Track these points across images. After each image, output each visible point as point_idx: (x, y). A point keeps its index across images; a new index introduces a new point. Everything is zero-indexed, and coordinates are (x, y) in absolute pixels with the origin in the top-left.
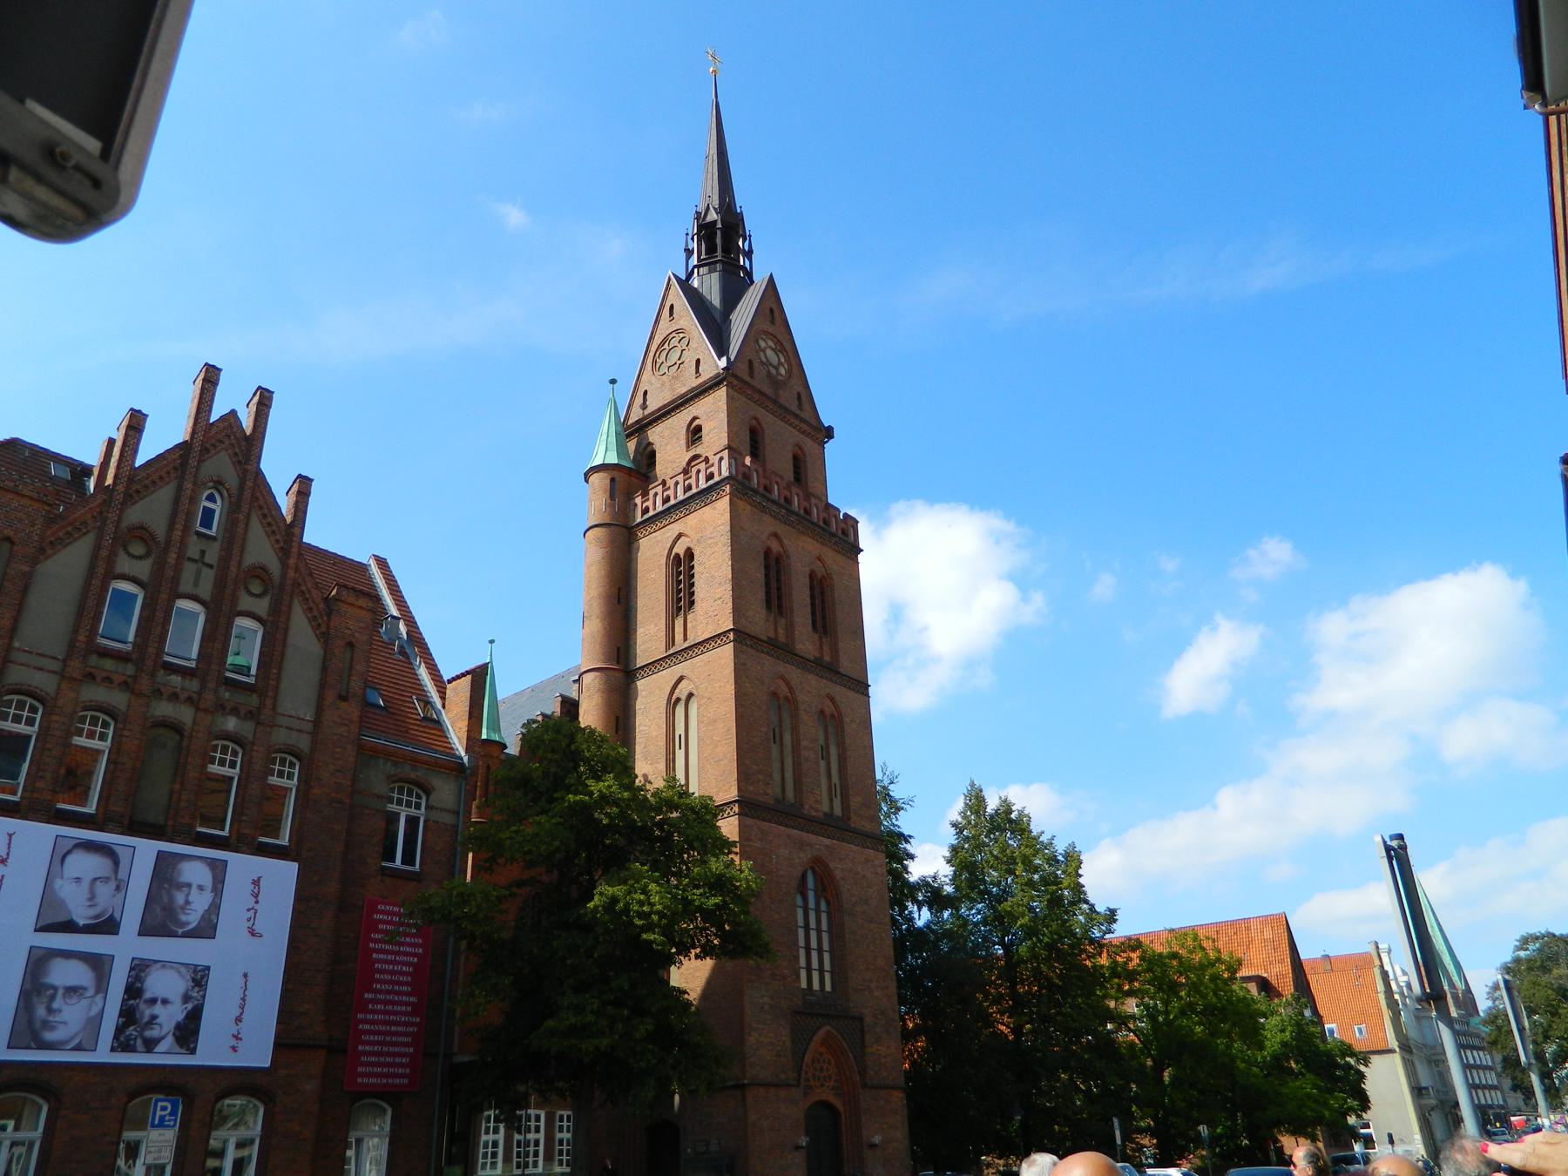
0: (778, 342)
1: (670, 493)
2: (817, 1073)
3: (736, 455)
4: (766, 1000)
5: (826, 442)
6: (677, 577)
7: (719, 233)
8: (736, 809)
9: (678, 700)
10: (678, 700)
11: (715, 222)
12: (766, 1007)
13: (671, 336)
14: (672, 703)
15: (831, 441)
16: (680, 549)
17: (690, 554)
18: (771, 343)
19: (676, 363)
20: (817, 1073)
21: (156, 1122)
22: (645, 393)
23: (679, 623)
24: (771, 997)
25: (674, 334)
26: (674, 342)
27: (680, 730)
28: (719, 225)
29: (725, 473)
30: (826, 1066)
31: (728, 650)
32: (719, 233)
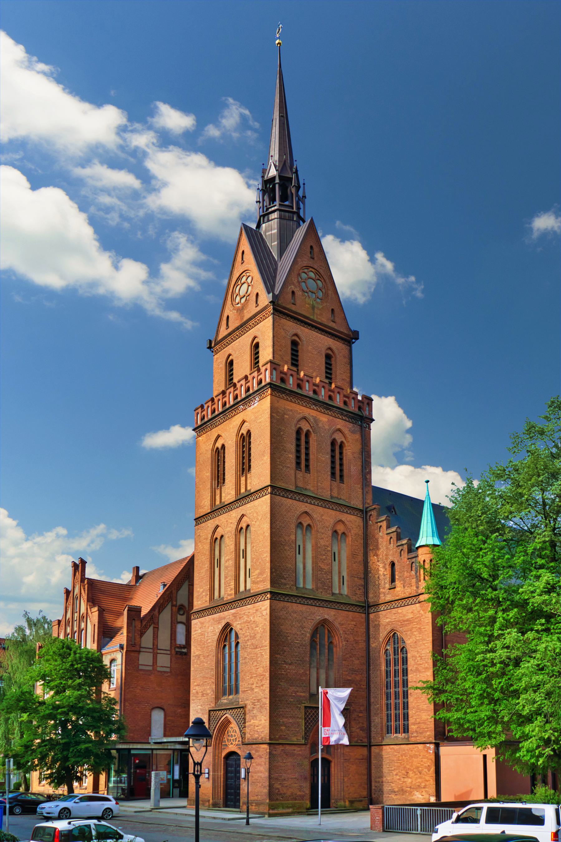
0: (317, 272)
1: (249, 384)
2: (230, 738)
3: (275, 366)
4: (199, 707)
5: (354, 343)
6: (243, 449)
7: (277, 186)
8: (269, 596)
9: (216, 539)
10: (216, 539)
11: (274, 178)
12: (199, 711)
13: (242, 276)
14: (239, 530)
15: (357, 341)
16: (244, 431)
17: (249, 433)
18: (312, 275)
19: (244, 296)
20: (230, 738)
21: (183, 753)
22: (228, 317)
23: (243, 479)
24: (201, 706)
25: (244, 274)
26: (244, 279)
27: (242, 547)
28: (277, 181)
29: (268, 380)
30: (233, 734)
31: (267, 498)
32: (277, 186)
